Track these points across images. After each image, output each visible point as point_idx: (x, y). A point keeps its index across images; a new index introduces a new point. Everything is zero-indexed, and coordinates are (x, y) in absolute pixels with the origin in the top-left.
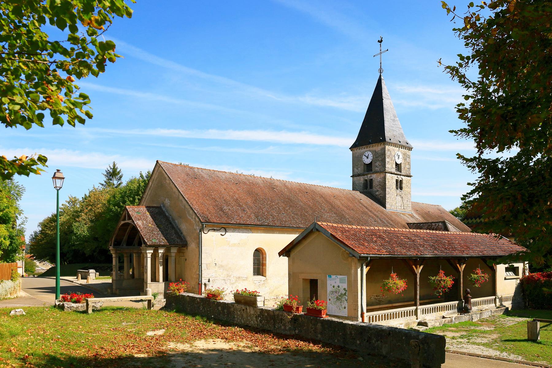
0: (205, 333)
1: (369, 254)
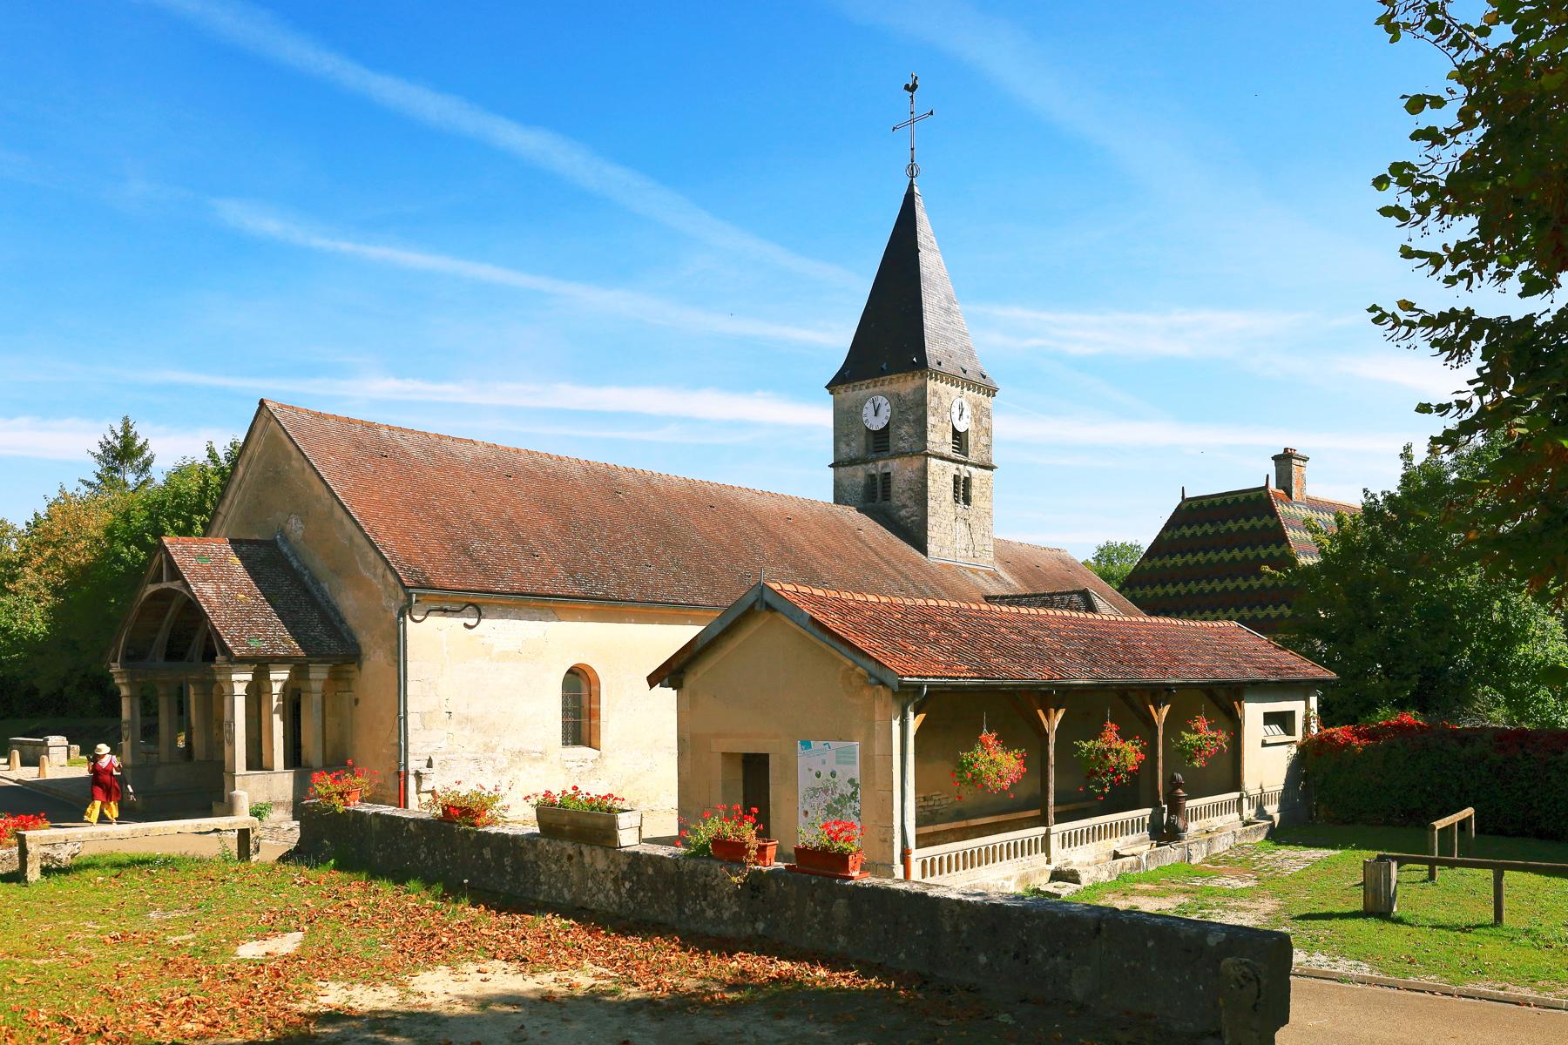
0: (445, 940)
1: (926, 677)
